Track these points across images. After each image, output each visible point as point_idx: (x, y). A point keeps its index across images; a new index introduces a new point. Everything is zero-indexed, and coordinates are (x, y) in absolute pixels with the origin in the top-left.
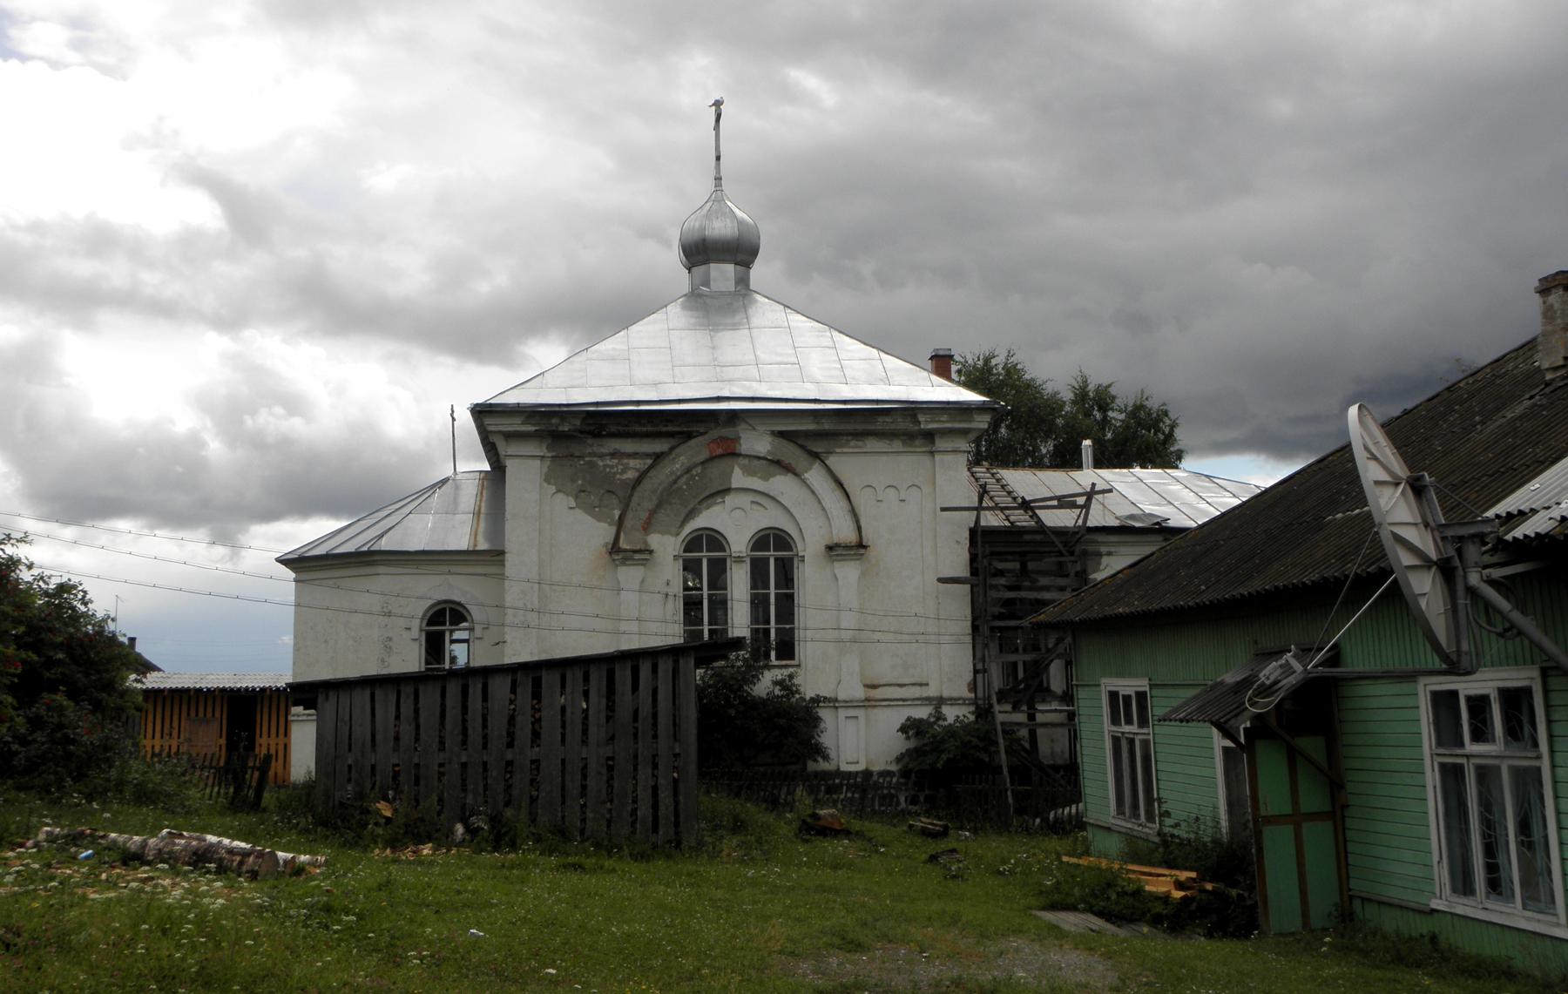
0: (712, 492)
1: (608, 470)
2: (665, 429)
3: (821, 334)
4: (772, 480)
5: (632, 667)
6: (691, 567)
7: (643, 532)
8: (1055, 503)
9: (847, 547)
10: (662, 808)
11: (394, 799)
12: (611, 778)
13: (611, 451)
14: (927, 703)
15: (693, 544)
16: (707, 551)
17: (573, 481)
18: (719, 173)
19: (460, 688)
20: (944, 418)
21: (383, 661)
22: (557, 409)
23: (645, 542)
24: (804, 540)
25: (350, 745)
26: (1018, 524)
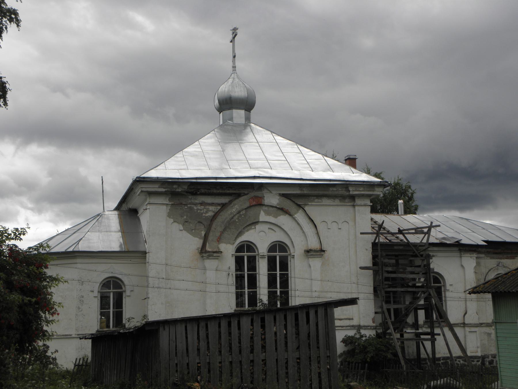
0: (250, 223)
1: (199, 211)
2: (228, 192)
3: (292, 146)
4: (279, 218)
5: (306, 312)
6: (239, 261)
7: (217, 242)
8: (413, 231)
9: (315, 251)
10: (323, 383)
11: (201, 380)
12: (299, 368)
13: (201, 202)
14: (353, 328)
15: (240, 249)
16: (247, 252)
17: (182, 217)
18: (235, 64)
19: (227, 323)
20: (361, 189)
21: (79, 308)
22: (177, 180)
23: (218, 248)
24: (294, 247)
25: (176, 353)
26: (392, 241)
